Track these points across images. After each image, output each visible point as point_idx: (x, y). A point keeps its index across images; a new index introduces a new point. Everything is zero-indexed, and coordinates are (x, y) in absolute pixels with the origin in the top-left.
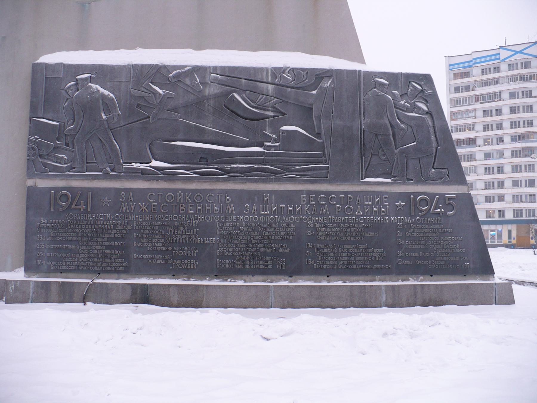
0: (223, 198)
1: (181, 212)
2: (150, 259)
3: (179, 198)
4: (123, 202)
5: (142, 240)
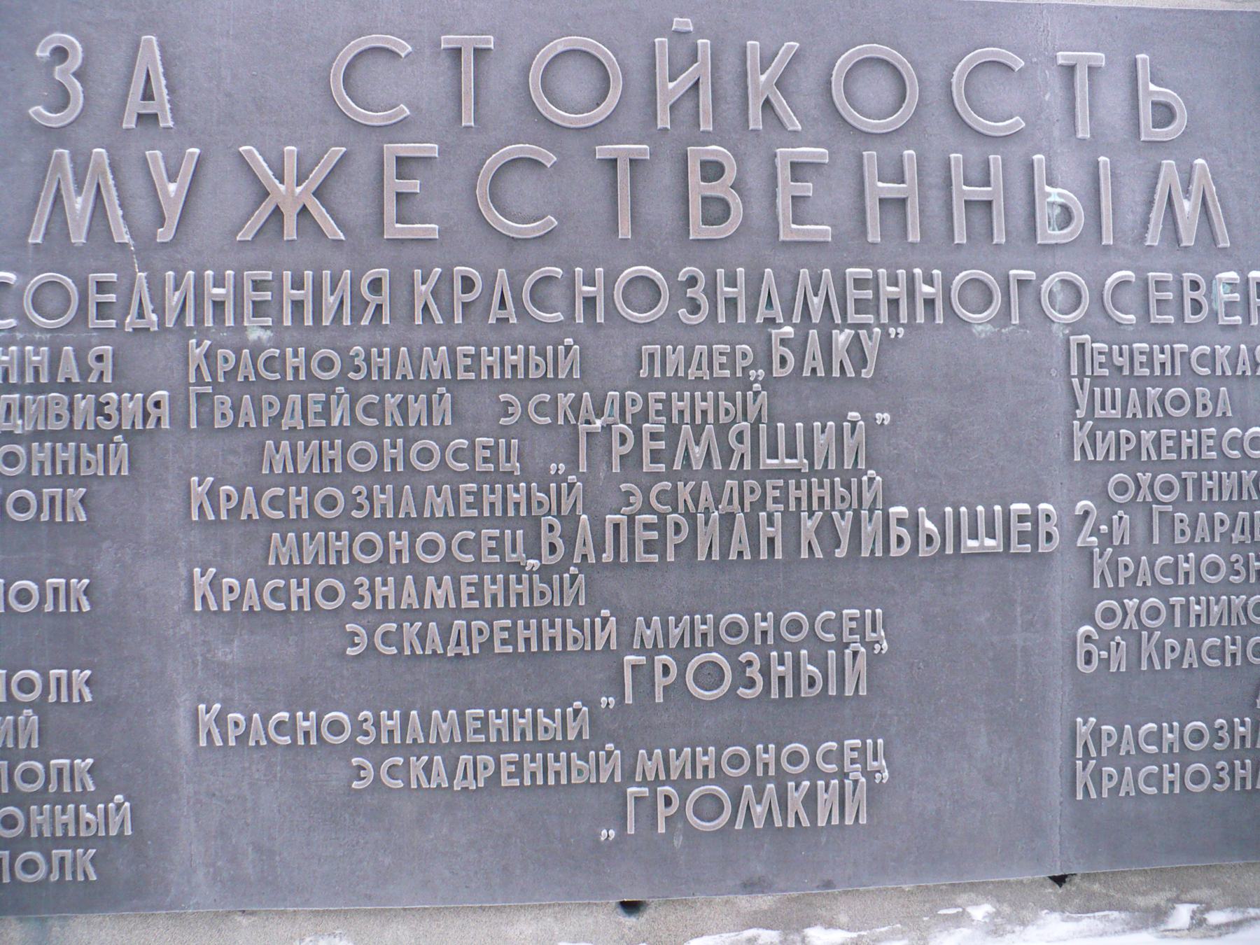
1: (698, 230)
2: (377, 751)
3: (671, 88)
4: (58, 136)
5: (282, 549)
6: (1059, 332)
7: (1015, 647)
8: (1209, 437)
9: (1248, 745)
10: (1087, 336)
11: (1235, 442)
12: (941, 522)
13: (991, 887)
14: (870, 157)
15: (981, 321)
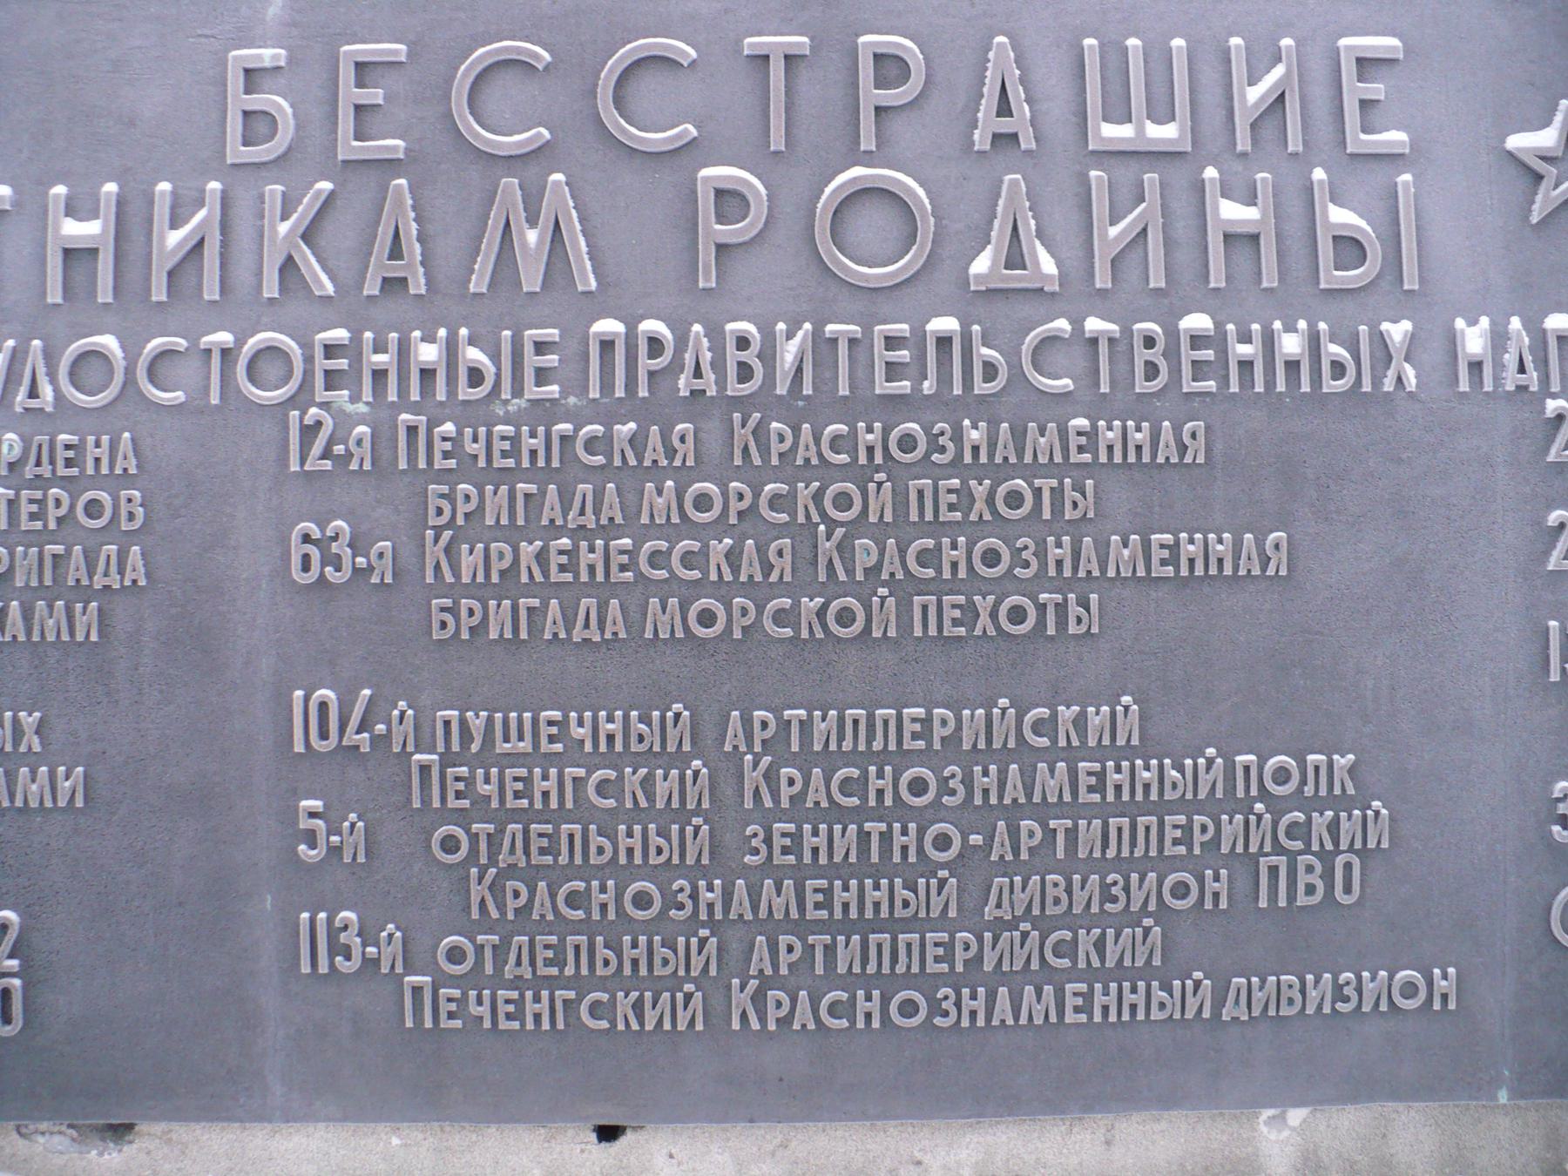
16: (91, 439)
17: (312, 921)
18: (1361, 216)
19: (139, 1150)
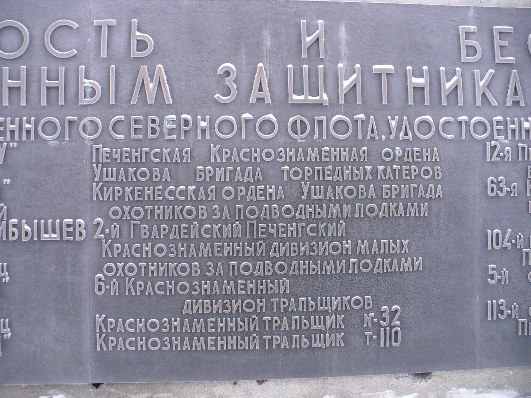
0: (120, 40)
6: (88, 143)
7: (67, 282)
8: (159, 190)
9: (178, 331)
10: (101, 145)
11: (171, 193)
12: (32, 227)
13: (64, 387)
14: (61, 68)
15: (51, 139)
16: (424, 150)
17: (4, 321)
18: (236, 68)
19: (433, 380)
